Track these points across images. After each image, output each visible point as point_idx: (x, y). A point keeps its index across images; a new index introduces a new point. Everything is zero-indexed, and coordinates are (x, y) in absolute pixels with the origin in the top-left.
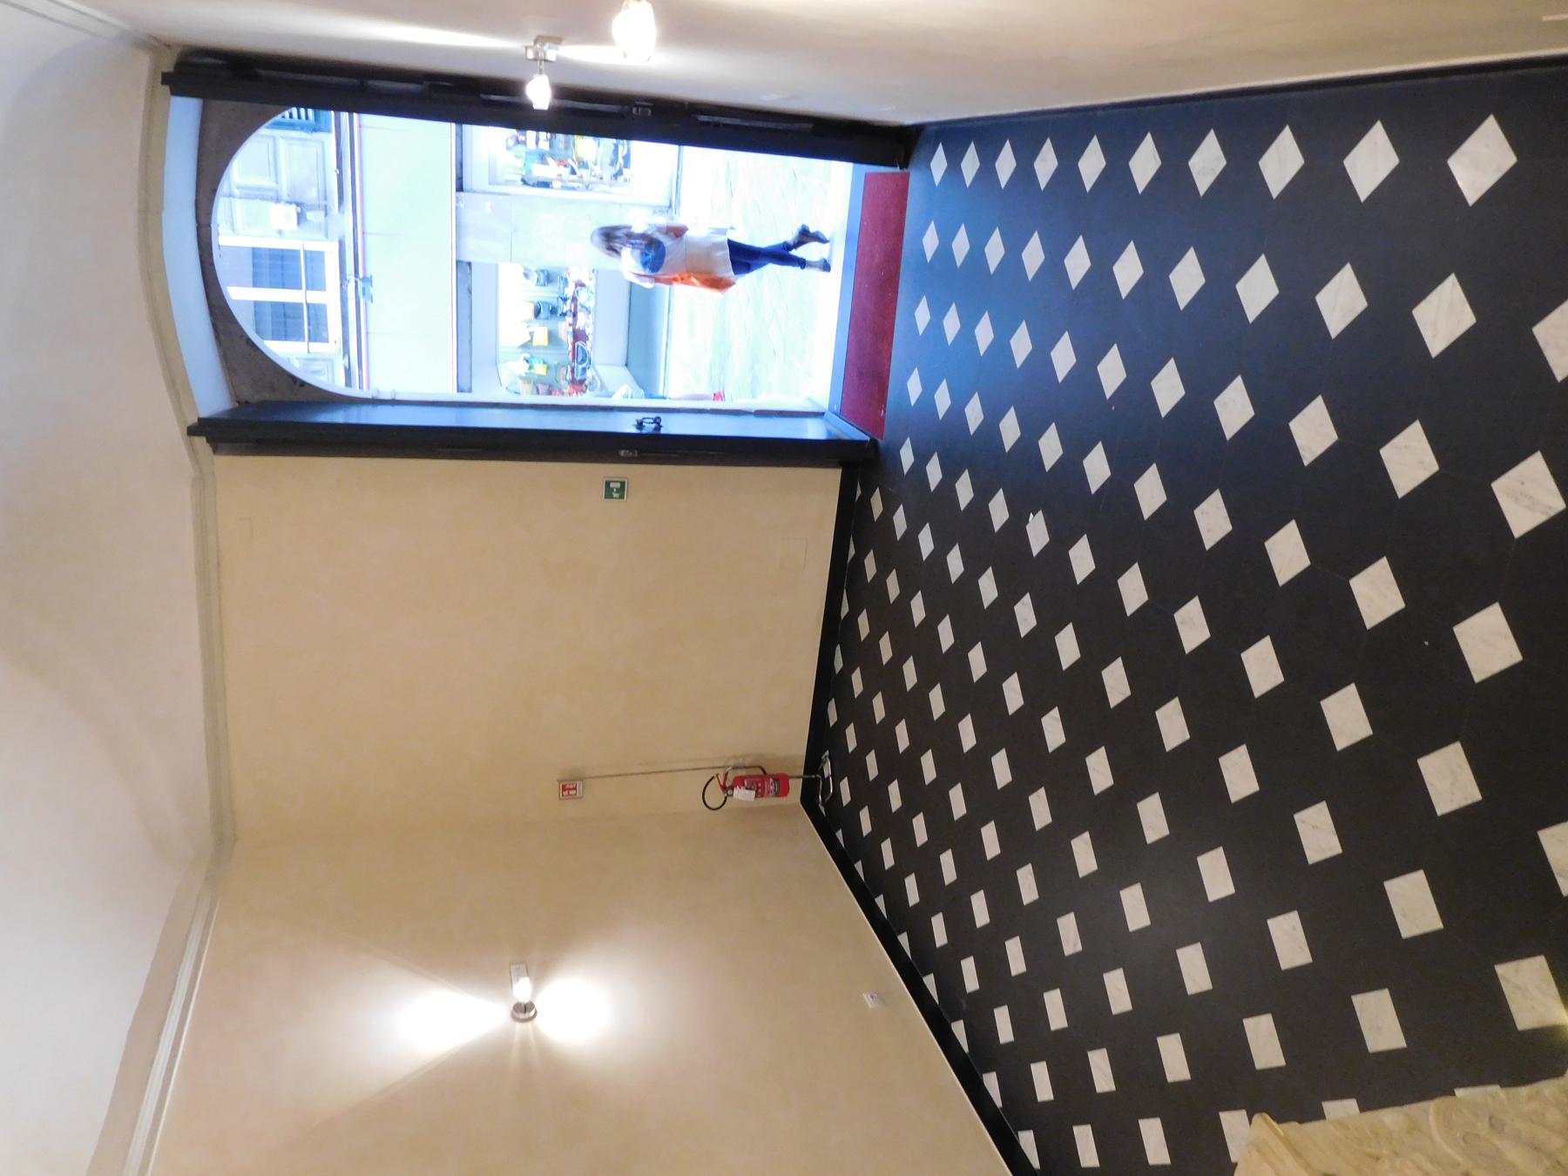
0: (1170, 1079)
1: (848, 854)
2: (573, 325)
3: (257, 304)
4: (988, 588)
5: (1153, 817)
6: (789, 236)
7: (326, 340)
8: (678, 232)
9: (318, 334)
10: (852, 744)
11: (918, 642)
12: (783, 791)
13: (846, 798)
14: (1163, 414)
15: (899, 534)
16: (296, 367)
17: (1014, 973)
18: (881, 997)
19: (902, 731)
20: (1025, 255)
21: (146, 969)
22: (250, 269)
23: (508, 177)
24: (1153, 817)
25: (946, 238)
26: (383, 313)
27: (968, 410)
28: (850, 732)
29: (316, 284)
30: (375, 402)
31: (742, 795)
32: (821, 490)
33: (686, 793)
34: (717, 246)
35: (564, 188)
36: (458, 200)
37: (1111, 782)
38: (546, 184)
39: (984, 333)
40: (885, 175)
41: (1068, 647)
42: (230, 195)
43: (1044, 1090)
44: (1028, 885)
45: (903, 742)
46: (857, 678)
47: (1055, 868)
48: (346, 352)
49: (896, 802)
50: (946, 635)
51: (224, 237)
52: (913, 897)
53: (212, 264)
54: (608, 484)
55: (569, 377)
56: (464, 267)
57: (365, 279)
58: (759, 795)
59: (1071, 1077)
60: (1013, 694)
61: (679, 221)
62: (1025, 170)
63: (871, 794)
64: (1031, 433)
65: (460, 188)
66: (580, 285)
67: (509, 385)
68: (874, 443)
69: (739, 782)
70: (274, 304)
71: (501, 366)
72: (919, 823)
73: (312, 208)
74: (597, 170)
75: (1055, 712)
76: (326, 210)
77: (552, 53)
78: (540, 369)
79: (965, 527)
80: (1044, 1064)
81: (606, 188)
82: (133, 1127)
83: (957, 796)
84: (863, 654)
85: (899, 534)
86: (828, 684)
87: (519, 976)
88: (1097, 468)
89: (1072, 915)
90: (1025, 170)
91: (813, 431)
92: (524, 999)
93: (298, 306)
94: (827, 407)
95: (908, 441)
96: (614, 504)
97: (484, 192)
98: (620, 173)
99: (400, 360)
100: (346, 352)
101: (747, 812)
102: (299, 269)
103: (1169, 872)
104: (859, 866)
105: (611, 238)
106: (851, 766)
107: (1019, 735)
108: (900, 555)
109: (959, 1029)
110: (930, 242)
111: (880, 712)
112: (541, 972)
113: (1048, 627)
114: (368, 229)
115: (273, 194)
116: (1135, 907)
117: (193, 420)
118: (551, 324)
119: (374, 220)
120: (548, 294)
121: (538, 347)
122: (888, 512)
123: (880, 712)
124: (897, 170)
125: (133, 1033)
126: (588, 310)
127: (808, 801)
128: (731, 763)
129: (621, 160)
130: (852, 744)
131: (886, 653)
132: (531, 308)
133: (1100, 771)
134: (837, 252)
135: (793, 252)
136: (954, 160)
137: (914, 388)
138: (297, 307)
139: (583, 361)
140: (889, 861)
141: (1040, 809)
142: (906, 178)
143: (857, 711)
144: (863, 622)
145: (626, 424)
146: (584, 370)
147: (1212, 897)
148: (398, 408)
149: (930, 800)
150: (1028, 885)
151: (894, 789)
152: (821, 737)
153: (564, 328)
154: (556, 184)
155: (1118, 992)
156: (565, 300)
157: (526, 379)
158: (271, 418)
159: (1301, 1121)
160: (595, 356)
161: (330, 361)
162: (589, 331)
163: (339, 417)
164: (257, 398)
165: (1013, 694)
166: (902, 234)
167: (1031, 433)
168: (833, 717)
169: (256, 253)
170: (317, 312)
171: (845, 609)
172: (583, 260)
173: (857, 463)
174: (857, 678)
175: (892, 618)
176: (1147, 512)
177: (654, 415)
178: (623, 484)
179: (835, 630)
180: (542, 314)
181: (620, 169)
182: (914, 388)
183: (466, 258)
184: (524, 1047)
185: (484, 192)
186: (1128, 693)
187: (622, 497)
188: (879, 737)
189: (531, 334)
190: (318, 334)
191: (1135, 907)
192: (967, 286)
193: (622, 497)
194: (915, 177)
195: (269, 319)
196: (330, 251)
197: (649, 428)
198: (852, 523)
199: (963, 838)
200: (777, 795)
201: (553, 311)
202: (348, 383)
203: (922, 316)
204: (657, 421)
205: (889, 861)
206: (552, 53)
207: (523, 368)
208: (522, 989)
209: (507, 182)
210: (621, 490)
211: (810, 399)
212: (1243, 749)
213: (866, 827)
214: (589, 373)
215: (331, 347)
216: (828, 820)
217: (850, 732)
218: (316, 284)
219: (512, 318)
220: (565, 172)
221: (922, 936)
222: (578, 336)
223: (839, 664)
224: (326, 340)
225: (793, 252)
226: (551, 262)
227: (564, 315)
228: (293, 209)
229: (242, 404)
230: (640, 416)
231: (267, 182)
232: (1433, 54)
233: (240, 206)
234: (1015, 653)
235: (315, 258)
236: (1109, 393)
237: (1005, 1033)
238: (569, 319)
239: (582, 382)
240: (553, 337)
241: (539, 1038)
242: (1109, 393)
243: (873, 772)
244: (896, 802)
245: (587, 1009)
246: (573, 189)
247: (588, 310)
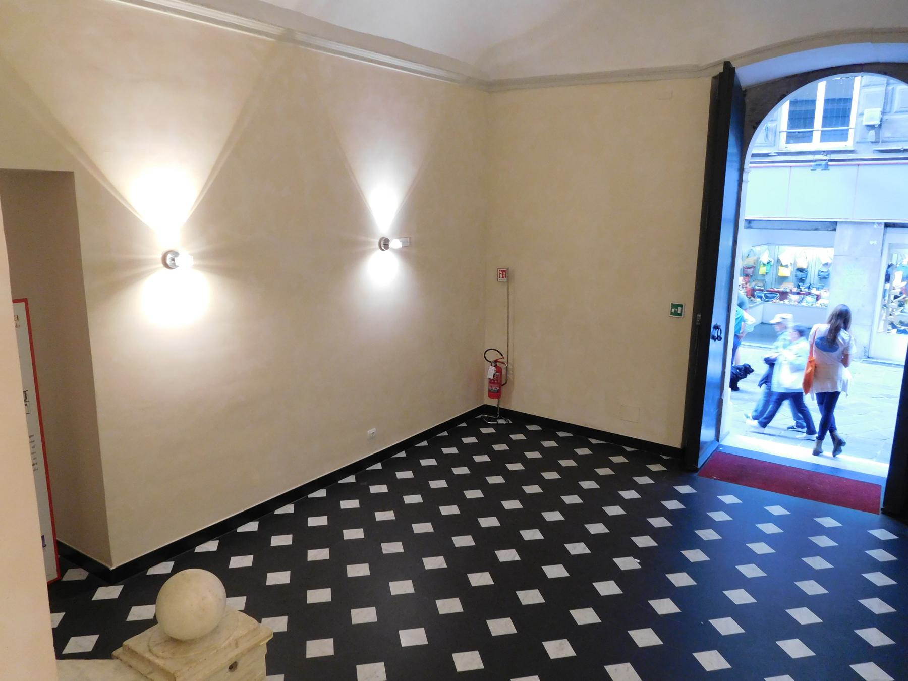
0: (309, 592)
1: (452, 429)
2: (791, 292)
3: (813, 102)
4: (597, 528)
5: (449, 606)
6: (840, 432)
7: (787, 142)
8: (845, 361)
9: (791, 137)
10: (514, 437)
11: (569, 482)
12: (492, 394)
13: (484, 431)
14: (695, 655)
15: (636, 479)
16: (767, 123)
17: (376, 513)
18: (373, 437)
19: (518, 467)
20: (812, 582)
21: (424, 48)
22: (837, 97)
23: (895, 256)
24: (449, 606)
25: (830, 532)
26: (805, 177)
27: (711, 531)
28: (521, 437)
29: (825, 137)
30: (741, 170)
31: (492, 371)
32: (669, 435)
33: (495, 339)
34: (835, 384)
35: (885, 291)
36: (879, 224)
37: (473, 585)
38: (888, 279)
39: (761, 548)
40: (879, 498)
41: (555, 571)
42: (888, 84)
43: (313, 522)
44: (422, 528)
45: (512, 467)
46: (552, 444)
47: (431, 545)
48: (779, 154)
49: (478, 458)
50: (572, 500)
51: (859, 80)
52: (424, 462)
53: (836, 73)
54: (681, 306)
55: (757, 288)
56: (833, 226)
57: (827, 165)
58: (490, 381)
59: (318, 538)
60: (531, 535)
61: (853, 363)
63: (484, 445)
65: (887, 225)
66: (818, 298)
67: (748, 250)
68: (696, 470)
69: (499, 370)
70: (813, 111)
71: (766, 247)
72: (465, 470)
73: (877, 134)
74: (897, 313)
75: (517, 558)
76: (876, 142)
78: (763, 270)
79: (636, 519)
80: (326, 523)
81: (884, 318)
82: (348, 44)
83: (477, 494)
84: (566, 449)
85: (636, 479)
86: (550, 427)
87: (403, 242)
88: (665, 607)
89: (402, 550)
91: (706, 434)
92: (391, 244)
93: (811, 125)
94: (722, 443)
95: (694, 491)
97: (883, 240)
98: (894, 326)
99: (772, 183)
100: (779, 154)
101: (482, 373)
102: (836, 125)
103: (418, 611)
104: (445, 434)
105: (842, 319)
106: (502, 435)
107: (507, 535)
108: (623, 478)
109: (351, 479)
110: (829, 522)
111: (530, 455)
112: (405, 254)
113: (621, 577)
114: (793, 169)
115: (888, 110)
116: (402, 587)
117: (734, 64)
118: (793, 279)
119: (868, 172)
120: (812, 277)
121: (777, 270)
122: (651, 474)
123: (530, 455)
124: (881, 507)
125: (393, 42)
126: (800, 301)
127: (485, 409)
128: (510, 367)
129: (903, 328)
130: (514, 437)
131: (565, 463)
132: (805, 267)
133: (480, 579)
134: (826, 460)
135: (828, 433)
136: (886, 545)
137: (729, 499)
138: (811, 124)
139: (767, 297)
140: (446, 451)
141: (463, 541)
142: (874, 511)
143: (533, 442)
144: (585, 451)
145: (717, 318)
146: (761, 297)
147: (401, 632)
148: (736, 184)
149: (476, 478)
150: (422, 528)
151: (485, 458)
152: (520, 420)
153: (789, 286)
154: (888, 286)
155: (358, 570)
156: (809, 288)
157: (757, 261)
158: (733, 110)
159: (267, 657)
160: (769, 304)
161: (774, 144)
162: (786, 301)
163: (732, 149)
164: (747, 101)
165: (531, 535)
166: (838, 505)
168: (531, 428)
169: (848, 101)
170: (807, 137)
171: (594, 441)
172: (832, 299)
173: (684, 458)
174: (552, 444)
175: (586, 469)
176: (632, 633)
177: (723, 336)
178: (680, 315)
179: (582, 434)
180: (800, 274)
182: (729, 499)
183: (838, 227)
184: (366, 243)
185: (883, 240)
186: (523, 603)
187: (672, 313)
188: (516, 453)
189: (787, 266)
190: (791, 137)
191: (402, 587)
192: (795, 541)
193: (672, 313)
194: (877, 517)
195: (803, 108)
196: (848, 145)
197: (714, 333)
198: (645, 451)
199: (453, 495)
200: (489, 391)
201: (802, 280)
202: (754, 156)
203: (777, 510)
204: (719, 338)
205: (446, 451)
207: (765, 259)
208: (396, 244)
209: (890, 256)
210: (676, 314)
211: (728, 433)
212: (482, 667)
213: (466, 440)
214: (759, 300)
215: (783, 145)
216: (473, 419)
217: (521, 437)
218: (825, 137)
219: (795, 255)
220: (897, 291)
221: (403, 465)
222: (784, 295)
223: (561, 434)
224: (787, 142)
225: (828, 433)
226: (834, 280)
227: (799, 287)
228: (877, 122)
229: (743, 93)
230: (723, 328)
231: (896, 106)
233: (881, 89)
234: (555, 539)
235: (843, 136)
236: (713, 622)
237: (346, 504)
238: (795, 290)
239: (753, 296)
240: (783, 279)
241: (370, 251)
242: (713, 622)
243: (497, 447)
244: (478, 458)
245: (383, 276)
246: (884, 296)
247: (800, 301)
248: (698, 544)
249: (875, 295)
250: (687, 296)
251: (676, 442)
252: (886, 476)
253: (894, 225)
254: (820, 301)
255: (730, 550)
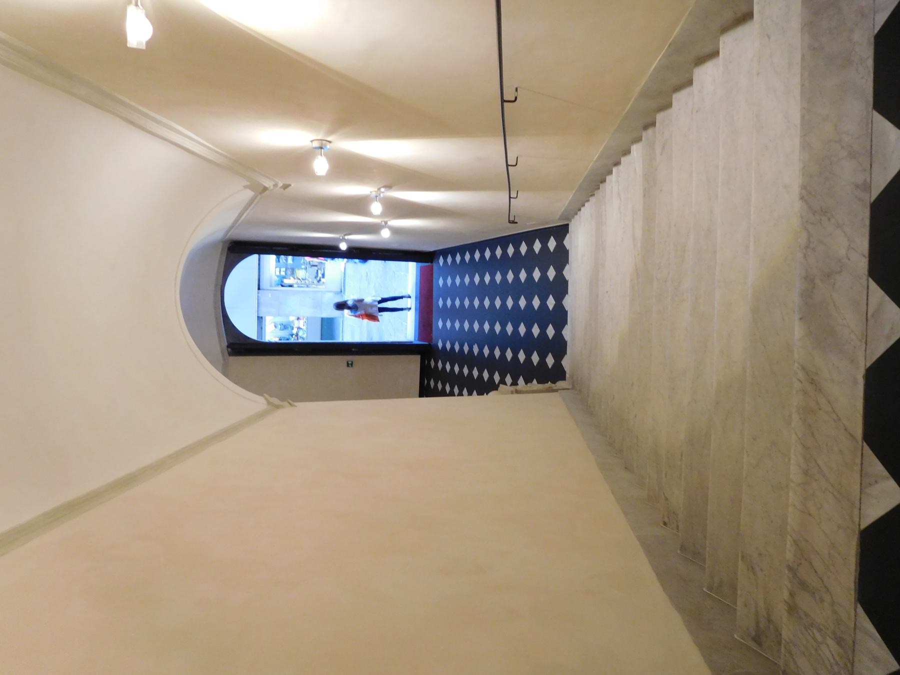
32: (414, 363)
38: (291, 286)
62: (463, 259)
64: (481, 349)
65: (259, 289)
66: (299, 328)
77: (346, 237)
90: (463, 259)
96: (350, 369)
129: (320, 275)
136: (445, 259)
156: (292, 335)
167: (481, 349)
181: (319, 278)
194: (435, 265)
206: (346, 237)
232: (543, 224)
248: (452, 348)
249: (302, 292)
250: (342, 360)
251: (417, 359)
252: (340, 340)
253: (259, 285)
254: (301, 326)
255: (452, 335)
